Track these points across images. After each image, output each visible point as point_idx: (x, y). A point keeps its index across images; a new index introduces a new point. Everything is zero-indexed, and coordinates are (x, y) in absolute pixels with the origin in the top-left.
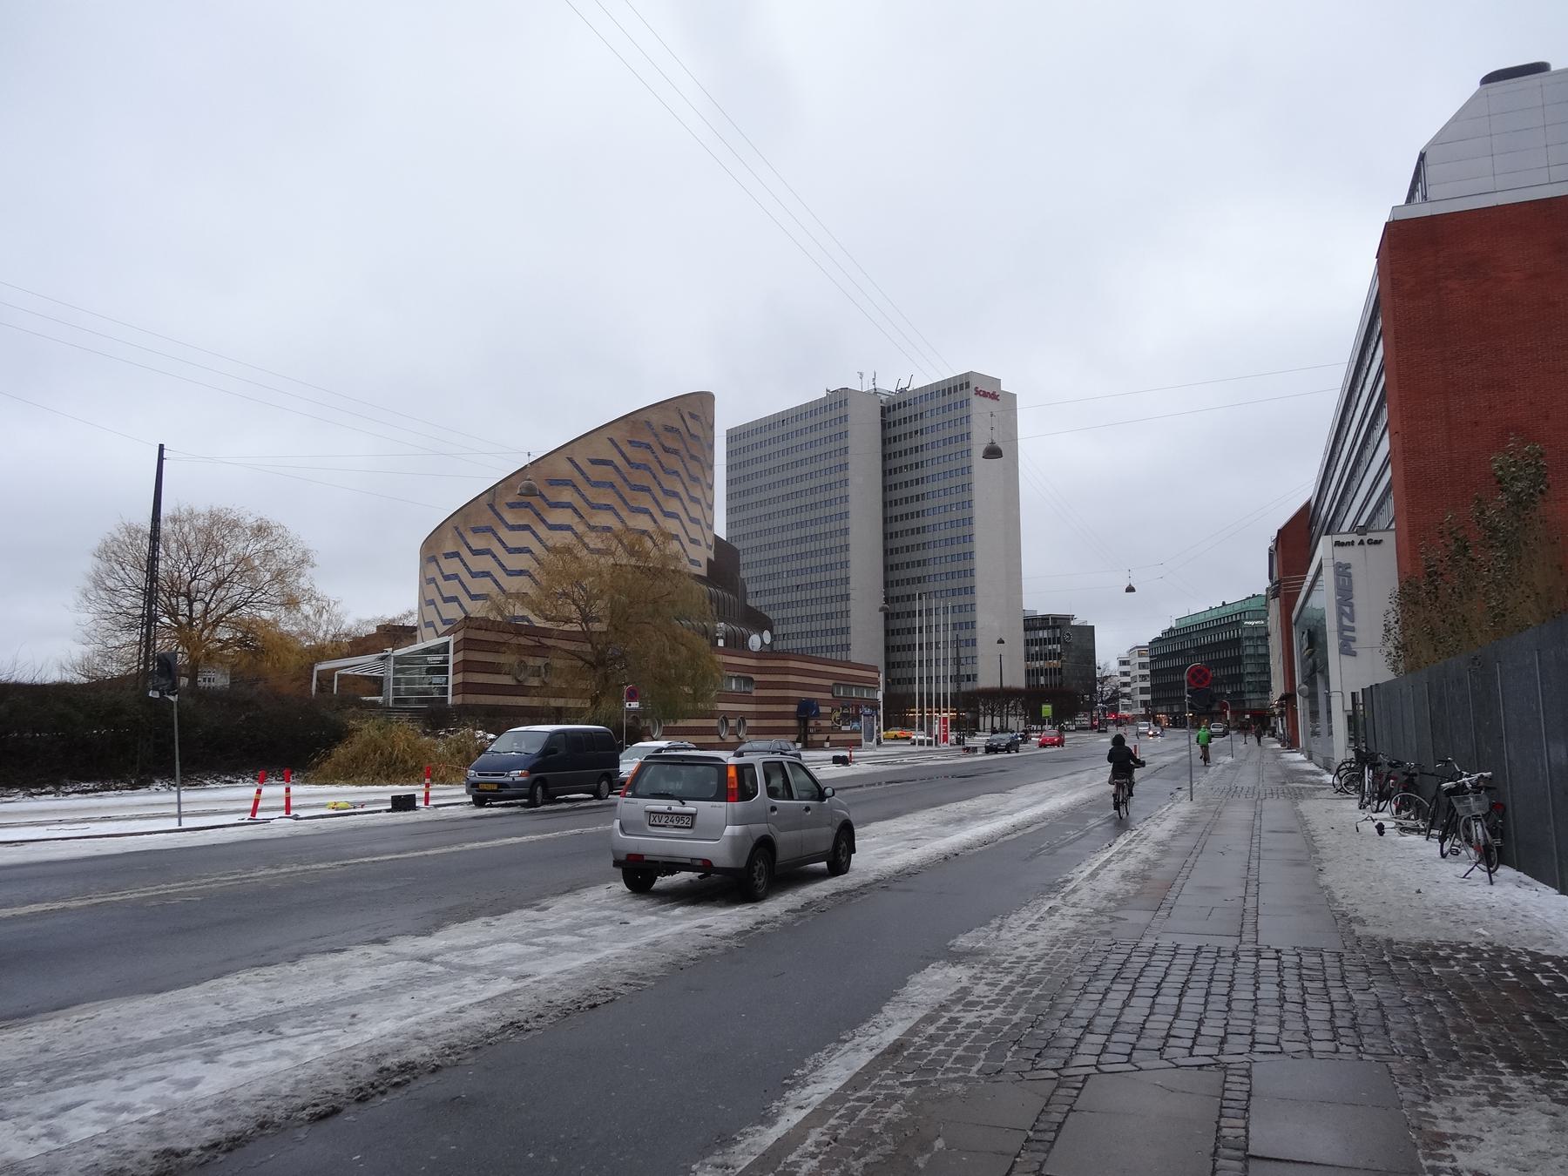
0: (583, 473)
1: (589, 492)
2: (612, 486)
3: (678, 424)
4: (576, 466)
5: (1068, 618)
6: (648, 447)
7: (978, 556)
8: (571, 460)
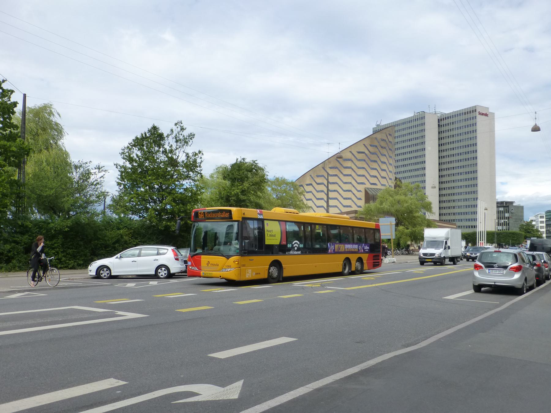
0: (355, 157)
1: (366, 166)
2: (365, 160)
3: (385, 138)
4: (353, 154)
5: (512, 203)
6: (376, 147)
7: (479, 179)
8: (351, 152)
